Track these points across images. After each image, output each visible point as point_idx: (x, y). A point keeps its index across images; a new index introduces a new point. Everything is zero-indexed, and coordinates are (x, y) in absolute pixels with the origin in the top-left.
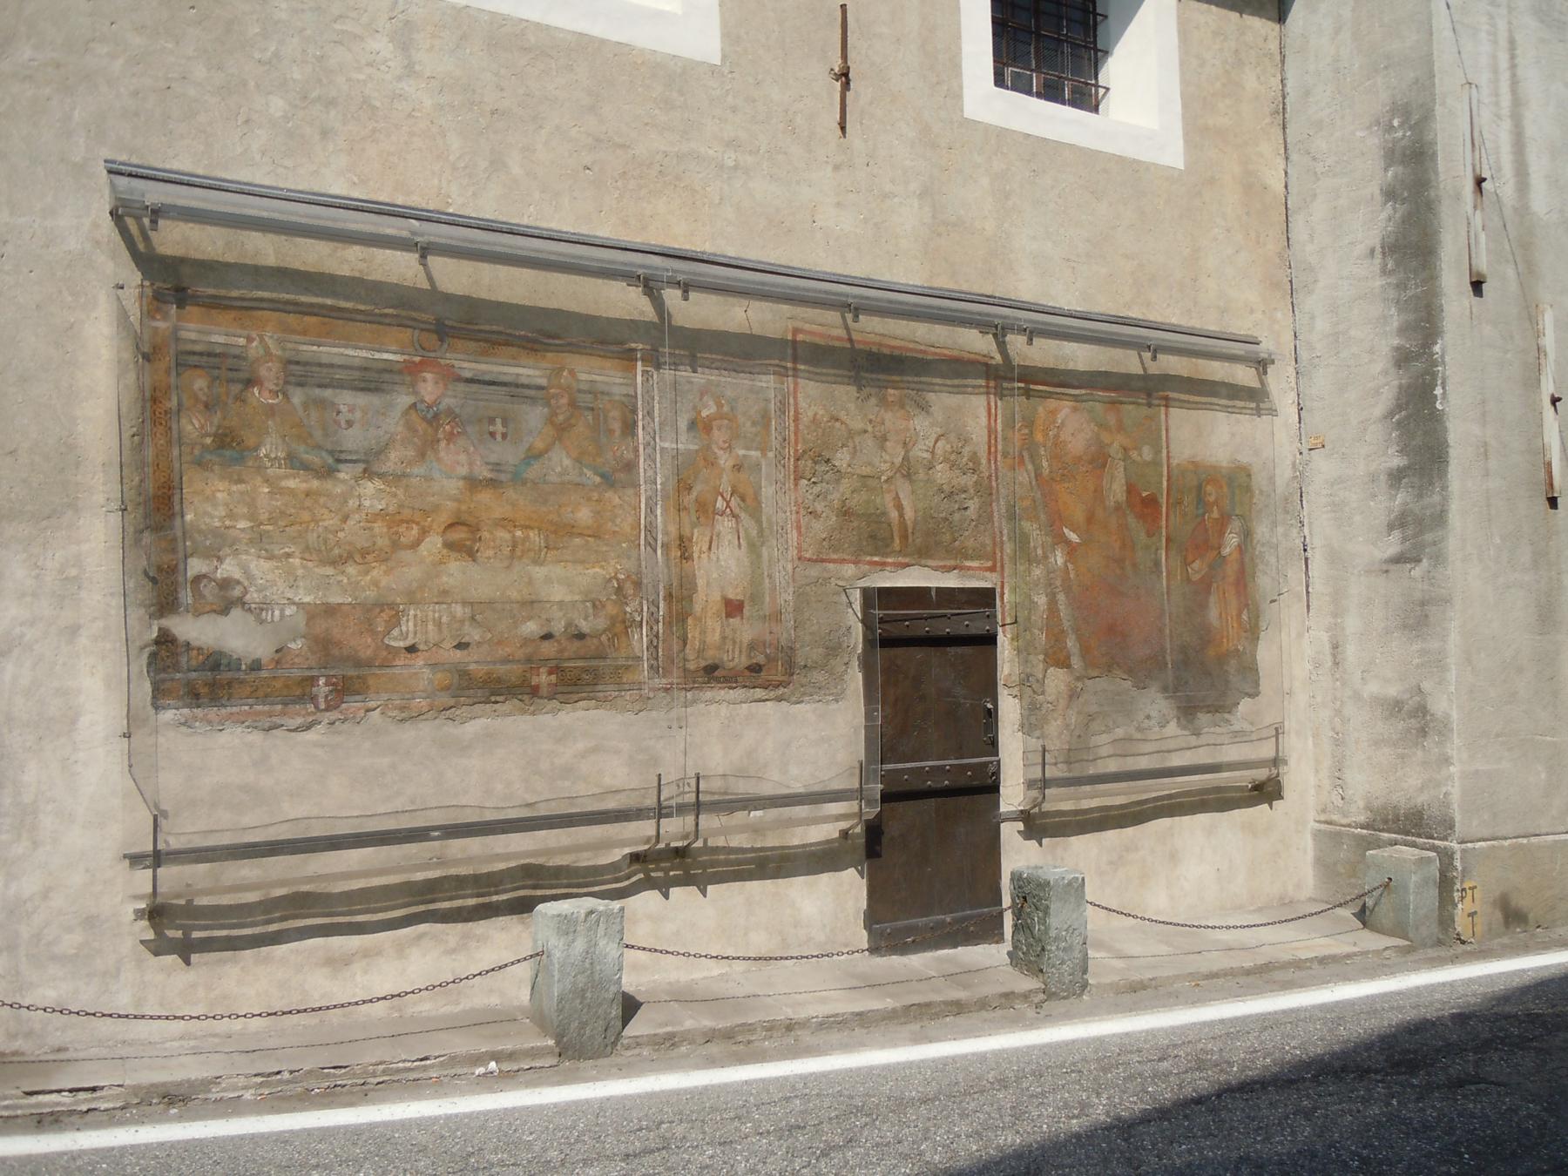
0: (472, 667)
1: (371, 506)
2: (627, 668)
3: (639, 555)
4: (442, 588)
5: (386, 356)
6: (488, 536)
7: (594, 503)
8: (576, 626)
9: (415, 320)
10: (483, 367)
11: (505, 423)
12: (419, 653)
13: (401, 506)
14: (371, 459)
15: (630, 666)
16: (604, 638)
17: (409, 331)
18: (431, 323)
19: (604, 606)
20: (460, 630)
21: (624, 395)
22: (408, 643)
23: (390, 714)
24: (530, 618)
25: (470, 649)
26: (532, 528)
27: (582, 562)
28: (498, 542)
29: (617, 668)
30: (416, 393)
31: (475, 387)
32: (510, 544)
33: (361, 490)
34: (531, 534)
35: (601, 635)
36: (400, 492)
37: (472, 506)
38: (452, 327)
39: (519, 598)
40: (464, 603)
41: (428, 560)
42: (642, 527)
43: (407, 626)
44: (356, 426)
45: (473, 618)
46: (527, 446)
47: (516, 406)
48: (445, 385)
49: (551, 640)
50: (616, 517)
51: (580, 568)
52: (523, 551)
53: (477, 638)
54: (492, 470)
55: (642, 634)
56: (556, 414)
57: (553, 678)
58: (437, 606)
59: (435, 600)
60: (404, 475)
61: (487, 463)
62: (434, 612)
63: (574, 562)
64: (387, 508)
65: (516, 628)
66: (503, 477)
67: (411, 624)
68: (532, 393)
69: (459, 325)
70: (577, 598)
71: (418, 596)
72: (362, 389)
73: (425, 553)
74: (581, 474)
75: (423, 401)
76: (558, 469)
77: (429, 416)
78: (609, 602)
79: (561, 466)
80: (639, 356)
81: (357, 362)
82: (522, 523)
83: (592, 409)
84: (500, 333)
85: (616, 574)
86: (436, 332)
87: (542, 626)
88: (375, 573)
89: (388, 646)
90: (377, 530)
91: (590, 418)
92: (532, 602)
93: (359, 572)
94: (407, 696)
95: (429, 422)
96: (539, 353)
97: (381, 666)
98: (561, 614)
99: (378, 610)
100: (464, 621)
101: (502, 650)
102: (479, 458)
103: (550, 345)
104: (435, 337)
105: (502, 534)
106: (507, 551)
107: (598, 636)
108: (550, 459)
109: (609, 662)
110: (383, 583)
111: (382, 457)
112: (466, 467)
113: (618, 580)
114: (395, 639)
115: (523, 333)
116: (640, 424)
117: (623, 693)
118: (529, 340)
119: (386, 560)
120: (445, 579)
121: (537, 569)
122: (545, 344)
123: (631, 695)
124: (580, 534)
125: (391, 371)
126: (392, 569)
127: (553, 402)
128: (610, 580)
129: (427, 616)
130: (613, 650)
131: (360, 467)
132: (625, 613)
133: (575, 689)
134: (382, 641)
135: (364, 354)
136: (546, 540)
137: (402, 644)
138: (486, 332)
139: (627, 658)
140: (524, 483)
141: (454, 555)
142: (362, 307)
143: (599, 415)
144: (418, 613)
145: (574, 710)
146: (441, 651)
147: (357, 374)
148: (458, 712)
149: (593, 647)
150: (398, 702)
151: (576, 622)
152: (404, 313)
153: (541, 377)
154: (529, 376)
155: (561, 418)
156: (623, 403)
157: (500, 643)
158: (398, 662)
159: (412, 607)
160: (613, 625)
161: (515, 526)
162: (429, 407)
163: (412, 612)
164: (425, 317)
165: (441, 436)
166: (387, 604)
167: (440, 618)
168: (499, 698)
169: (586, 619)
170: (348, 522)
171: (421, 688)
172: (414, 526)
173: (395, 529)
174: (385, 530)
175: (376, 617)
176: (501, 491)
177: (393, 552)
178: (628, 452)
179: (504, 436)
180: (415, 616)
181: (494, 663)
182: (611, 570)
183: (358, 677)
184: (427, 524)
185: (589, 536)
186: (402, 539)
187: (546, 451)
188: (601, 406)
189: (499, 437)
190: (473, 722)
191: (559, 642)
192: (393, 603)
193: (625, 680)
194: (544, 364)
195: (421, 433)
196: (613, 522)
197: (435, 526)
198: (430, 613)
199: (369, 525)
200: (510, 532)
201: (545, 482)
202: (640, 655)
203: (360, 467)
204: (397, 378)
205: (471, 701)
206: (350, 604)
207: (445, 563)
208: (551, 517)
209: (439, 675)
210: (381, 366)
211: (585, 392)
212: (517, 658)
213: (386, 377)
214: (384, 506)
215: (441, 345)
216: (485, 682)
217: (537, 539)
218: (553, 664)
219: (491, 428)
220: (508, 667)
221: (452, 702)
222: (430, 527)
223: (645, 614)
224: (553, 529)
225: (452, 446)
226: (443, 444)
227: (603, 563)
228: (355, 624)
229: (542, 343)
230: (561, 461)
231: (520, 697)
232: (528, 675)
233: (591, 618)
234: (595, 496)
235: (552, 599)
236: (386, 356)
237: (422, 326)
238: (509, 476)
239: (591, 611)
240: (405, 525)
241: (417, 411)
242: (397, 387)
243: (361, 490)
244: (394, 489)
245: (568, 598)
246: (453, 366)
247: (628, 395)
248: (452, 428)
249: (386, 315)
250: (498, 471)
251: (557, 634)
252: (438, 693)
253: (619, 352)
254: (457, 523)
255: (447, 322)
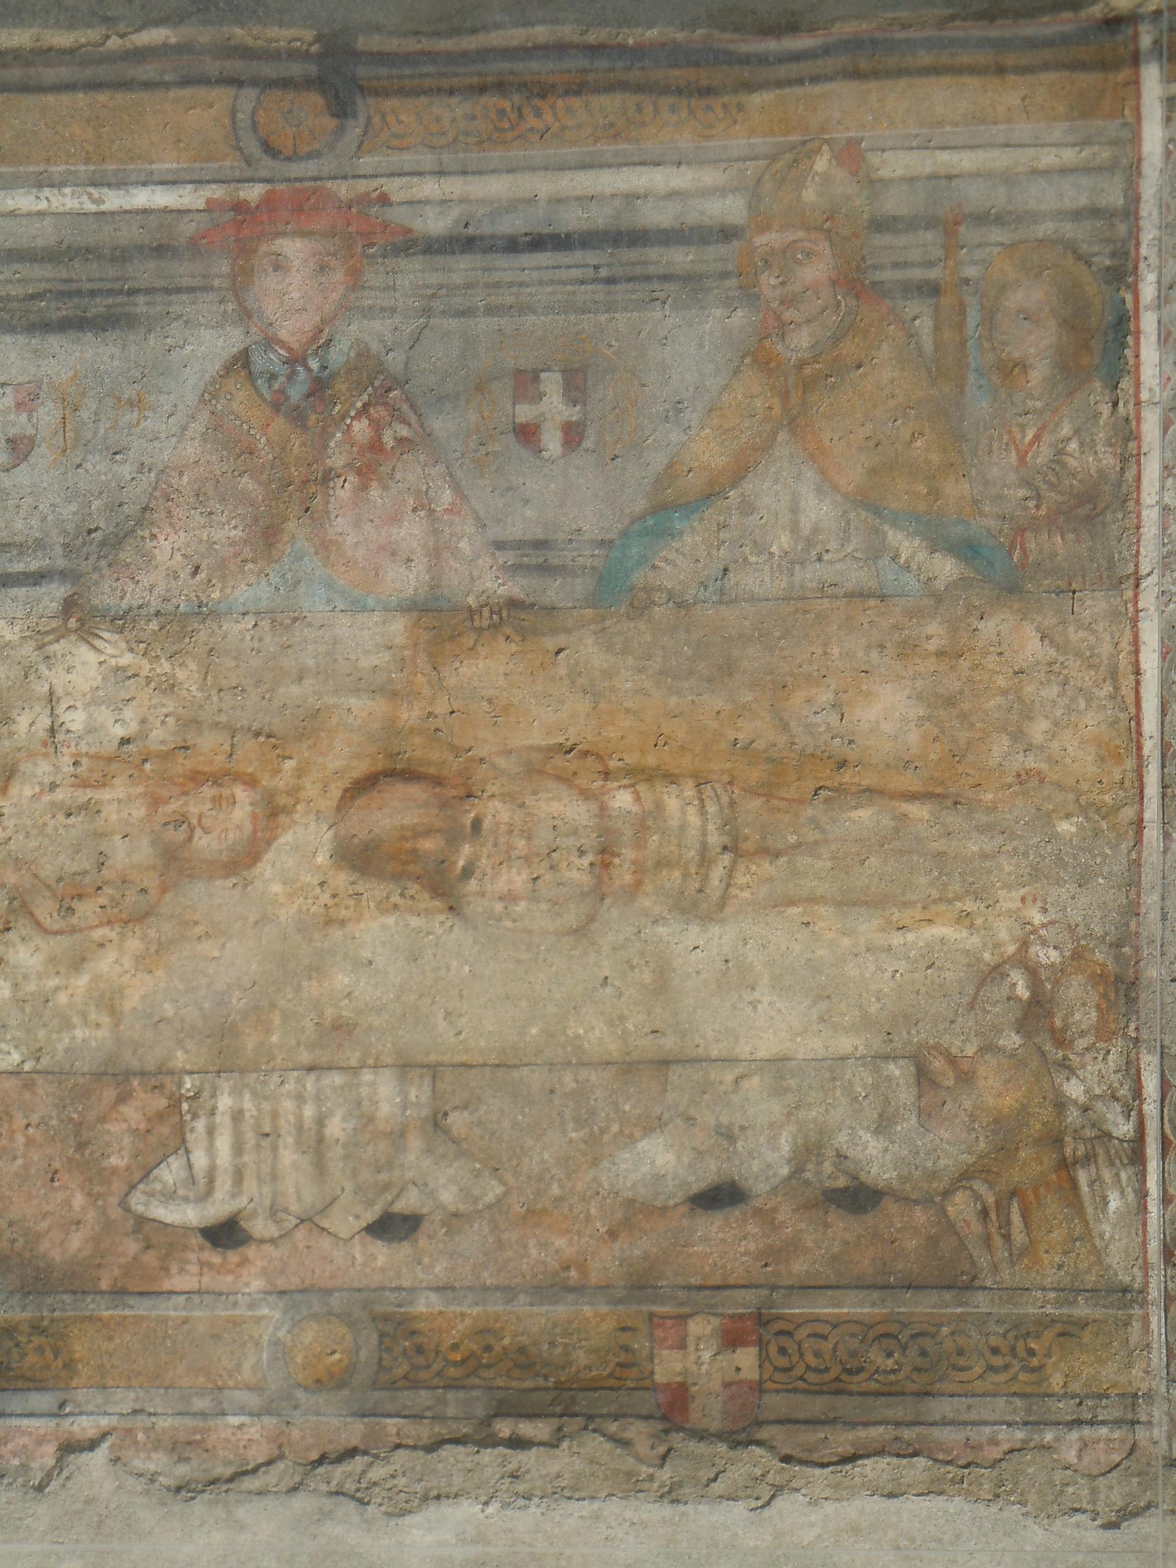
0: (426, 1304)
1: (91, 730)
2: (1070, 1331)
3: (1137, 864)
4: (329, 1012)
5: (142, 198)
6: (505, 817)
7: (931, 664)
8: (841, 1156)
9: (245, 53)
10: (497, 187)
11: (575, 389)
12: (251, 1251)
13: (191, 723)
14: (86, 566)
15: (1083, 1324)
16: (961, 1207)
17: (221, 96)
18: (306, 56)
19: (966, 1078)
20: (390, 1165)
21: (1077, 215)
22: (216, 1210)
23: (138, 1464)
24: (652, 1125)
25: (423, 1242)
26: (671, 778)
27: (876, 903)
28: (543, 837)
29: (1022, 1330)
30: (245, 315)
31: (462, 267)
32: (589, 840)
33: (57, 678)
34: (672, 804)
35: (946, 1194)
36: (188, 675)
37: (441, 707)
38: (381, 58)
39: (614, 1048)
40: (405, 1067)
41: (285, 915)
42: (1150, 747)
43: (211, 1149)
44: (43, 455)
45: (436, 1123)
46: (659, 461)
47: (623, 319)
48: (355, 273)
49: (736, 1212)
50: (1028, 715)
51: (868, 927)
52: (639, 868)
53: (448, 1196)
54: (517, 568)
55: (1143, 1194)
56: (783, 329)
57: (747, 1359)
58: (310, 1082)
59: (305, 1057)
60: (204, 612)
61: (500, 545)
62: (300, 1098)
63: (844, 903)
64: (143, 735)
65: (595, 1162)
66: (553, 591)
67: (224, 1143)
68: (681, 258)
69: (411, 45)
70: (845, 1044)
71: (250, 1043)
72: (66, 325)
73: (276, 888)
74: (876, 551)
75: (270, 342)
76: (783, 541)
77: (296, 393)
78: (992, 1060)
79: (795, 529)
80: (1146, 41)
81: (44, 235)
82: (632, 759)
83: (933, 290)
84: (560, 49)
85: (1025, 944)
86: (318, 83)
87: (700, 1154)
88: (105, 964)
89: (141, 1221)
90: (111, 814)
91: (925, 325)
92: (664, 1063)
93: (52, 960)
94: (199, 1404)
95: (298, 417)
96: (717, 103)
97: (119, 1293)
98: (776, 1108)
99: (110, 1094)
100: (403, 1134)
101: (543, 1245)
102: (470, 529)
103: (763, 60)
104: (315, 99)
105: (556, 807)
106: (577, 872)
107: (936, 1200)
108: (747, 507)
109: (981, 1303)
110: (132, 1001)
111: (127, 554)
112: (420, 566)
113: (1032, 972)
114: (169, 1196)
115: (652, 34)
116: (1149, 322)
117: (1049, 1437)
118: (674, 54)
119: (139, 918)
120: (342, 980)
121: (694, 934)
122: (746, 60)
123: (1085, 1445)
124: (873, 793)
125: (160, 250)
126: (162, 947)
127: (768, 280)
128: (997, 972)
129: (275, 1115)
130: (1001, 1253)
131: (54, 594)
132: (1060, 1104)
133: (845, 1406)
134: (124, 1204)
135: (67, 200)
136: (729, 824)
137: (191, 1215)
138: (508, 53)
139: (1069, 1292)
140: (639, 608)
141: (373, 890)
142: (62, 39)
143: (962, 310)
144: (248, 1104)
145: (841, 1492)
146: (325, 1243)
147: (41, 273)
148: (378, 1472)
149: (912, 1244)
150: (163, 1423)
151: (841, 1139)
152: (204, 35)
153: (722, 191)
154: (673, 194)
155: (801, 340)
156: (1071, 247)
157: (533, 1215)
158: (179, 1282)
159: (225, 1084)
160: (1005, 1150)
161: (606, 775)
162: (295, 360)
163: (225, 1102)
164: (280, 35)
165: (337, 460)
166: (142, 1074)
167: (320, 1122)
168: (526, 1429)
169: (883, 1126)
170: (14, 791)
171: (246, 1374)
172: (240, 792)
173: (174, 806)
174: (139, 811)
175: (102, 1119)
176: (551, 643)
177: (164, 890)
178: (1088, 446)
179: (573, 435)
180: (237, 1116)
181: (509, 1292)
182: (1004, 931)
183: (37, 1328)
184: (281, 782)
185: (912, 797)
186: (202, 841)
187: (739, 472)
188: (971, 272)
189: (552, 443)
190: (432, 1511)
191: (766, 1216)
192: (163, 1070)
193: (1056, 1381)
194: (738, 143)
195: (266, 455)
196: (1018, 735)
197: (310, 789)
198: (288, 1105)
199: (83, 795)
200: (586, 795)
201: (725, 598)
202: (1123, 1271)
203: (54, 594)
204: (184, 271)
205: (424, 1432)
206: (15, 1073)
207: (343, 923)
208: (745, 730)
209: (310, 1334)
210: (130, 234)
211: (912, 224)
212: (594, 1279)
213: (144, 272)
214: (133, 728)
215: (340, 131)
216: (472, 1365)
217: (693, 819)
218: (744, 1302)
219: (525, 413)
220: (561, 1310)
221: (353, 1432)
222: (294, 792)
223: (1151, 1109)
224: (756, 775)
225: (375, 493)
226: (343, 491)
227: (969, 905)
228: (30, 1142)
229: (730, 59)
230: (795, 509)
231: (613, 1427)
232: (641, 1345)
233: (908, 1124)
234: (935, 632)
235: (744, 1049)
236: (142, 198)
237: (269, 70)
238: (581, 585)
239: (905, 1095)
240: (208, 791)
241: (251, 377)
242: (181, 304)
243: (57, 678)
244: (165, 666)
245: (812, 1046)
246: (384, 200)
247: (1095, 212)
248: (377, 427)
249: (141, 55)
250: (545, 569)
251: (762, 1187)
252: (300, 1395)
253: (1065, 40)
254: (391, 774)
255: (361, 43)
